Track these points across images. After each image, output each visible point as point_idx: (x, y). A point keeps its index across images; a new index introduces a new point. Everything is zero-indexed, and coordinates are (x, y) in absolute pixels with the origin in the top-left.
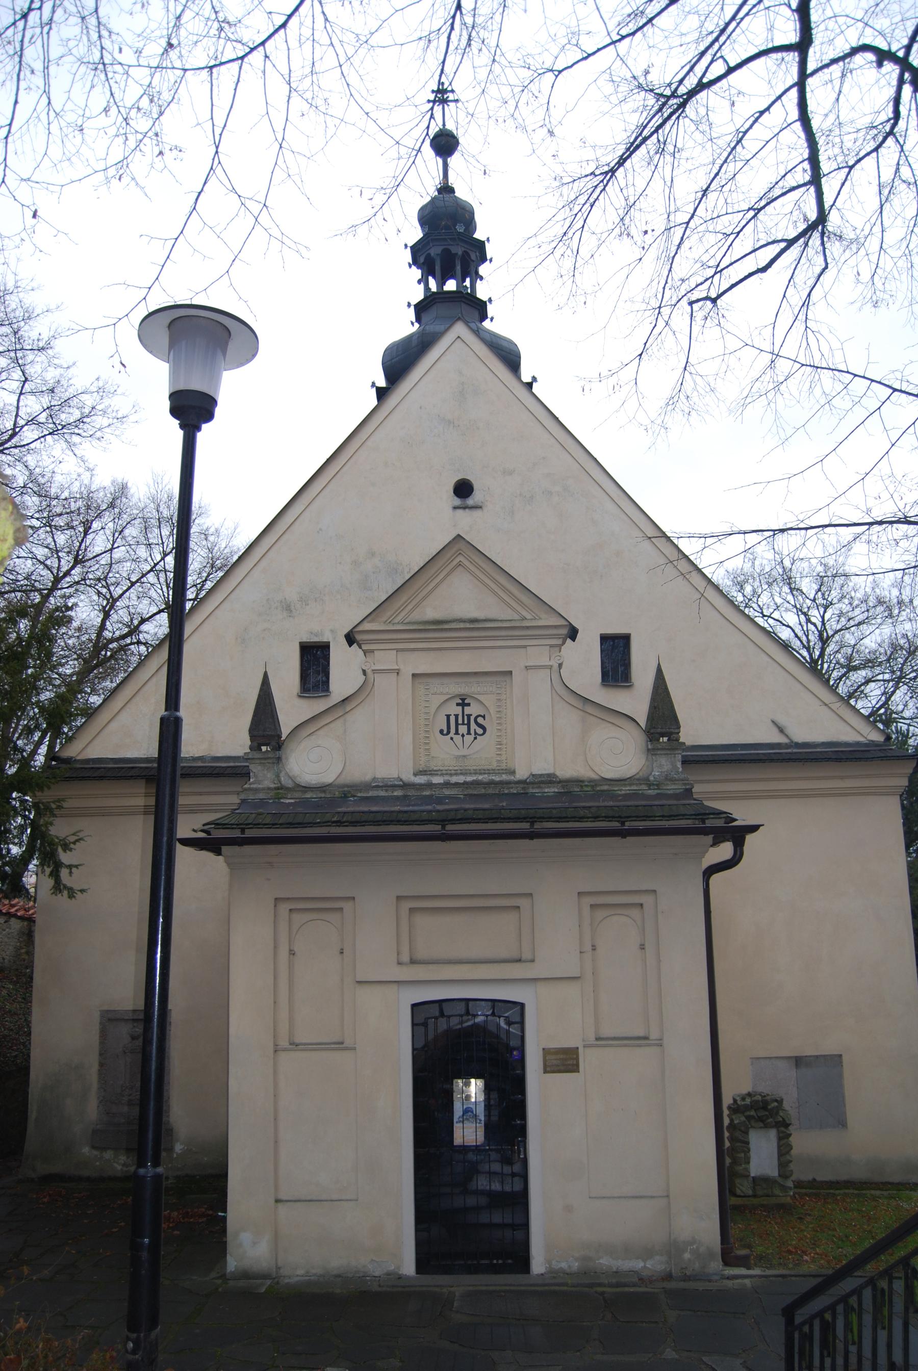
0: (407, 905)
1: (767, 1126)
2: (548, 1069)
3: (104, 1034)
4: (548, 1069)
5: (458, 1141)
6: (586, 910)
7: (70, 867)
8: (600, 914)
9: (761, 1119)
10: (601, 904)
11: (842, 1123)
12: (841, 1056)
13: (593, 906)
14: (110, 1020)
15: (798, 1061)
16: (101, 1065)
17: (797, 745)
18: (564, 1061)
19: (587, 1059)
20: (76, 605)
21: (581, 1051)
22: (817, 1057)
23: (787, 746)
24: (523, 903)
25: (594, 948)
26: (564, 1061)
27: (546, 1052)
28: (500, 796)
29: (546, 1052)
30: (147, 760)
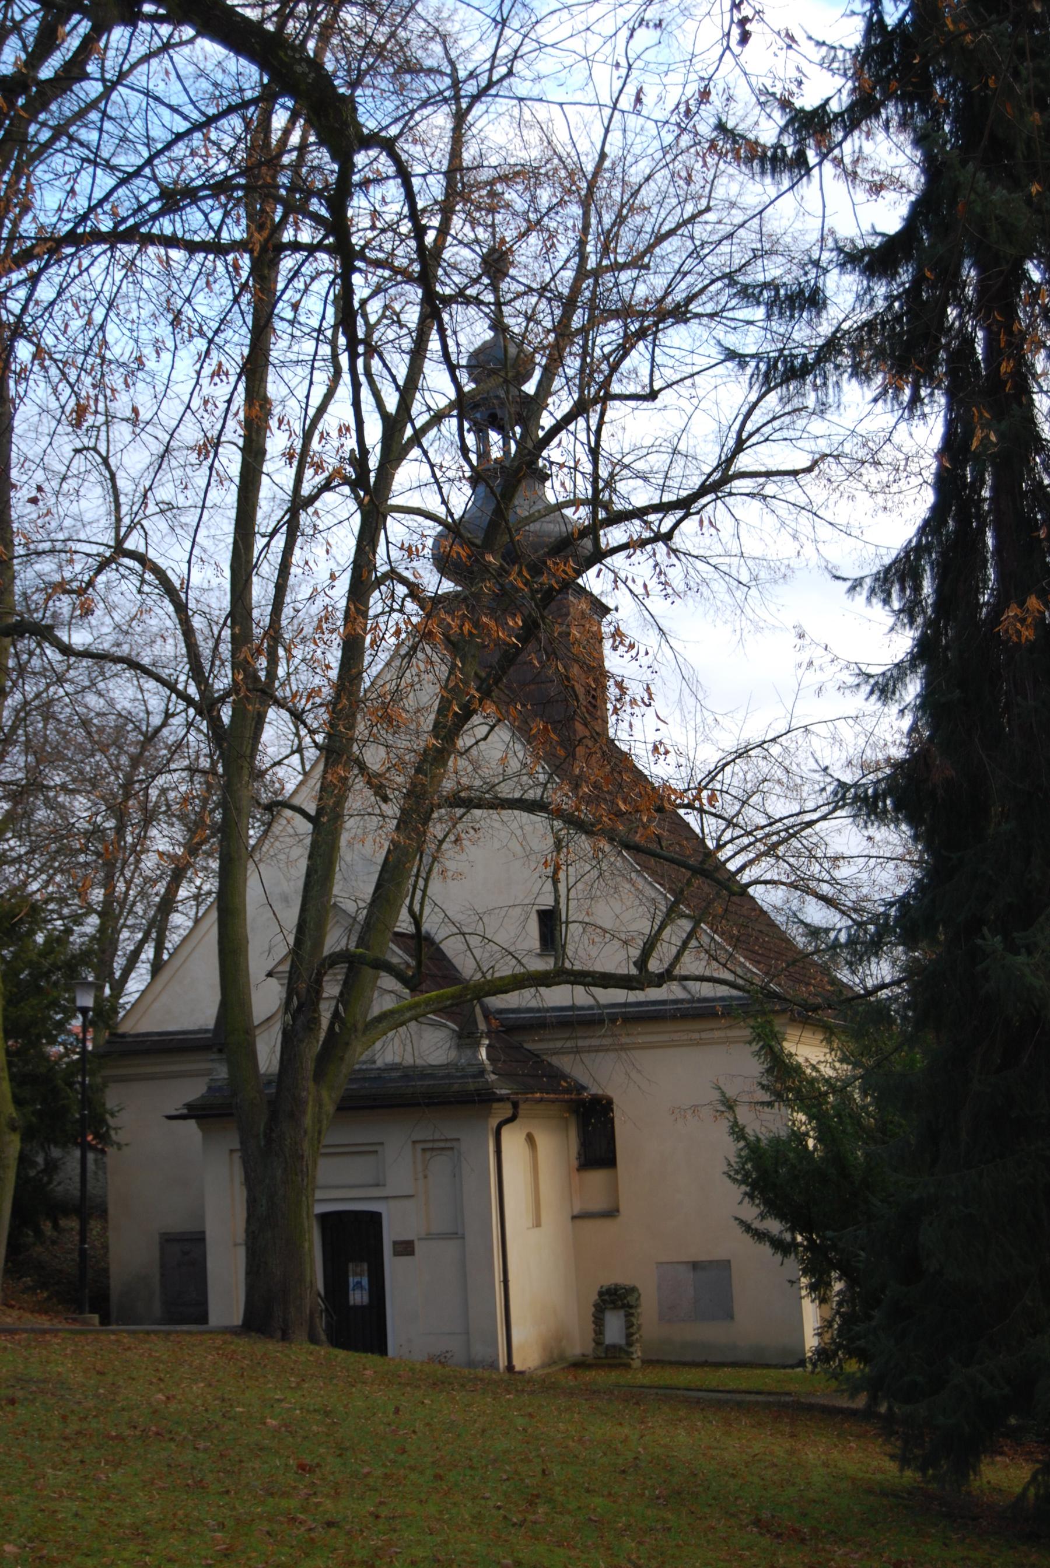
0: (419, 1146)
1: (616, 1308)
2: (396, 1253)
3: (162, 1249)
4: (396, 1253)
5: (352, 1303)
6: (419, 1153)
7: (115, 1129)
8: (428, 1155)
9: (613, 1302)
10: (430, 1149)
11: (731, 1317)
12: (729, 1261)
13: (424, 1150)
14: (167, 1241)
15: (695, 1266)
16: (162, 1275)
17: (699, 1000)
18: (405, 1248)
19: (418, 1247)
20: (764, 97)
21: (416, 1243)
22: (711, 1262)
23: (689, 1001)
24: (455, 1144)
25: (426, 1177)
26: (405, 1248)
27: (395, 1243)
28: (364, 1079)
29: (395, 1243)
30: (206, 1031)
